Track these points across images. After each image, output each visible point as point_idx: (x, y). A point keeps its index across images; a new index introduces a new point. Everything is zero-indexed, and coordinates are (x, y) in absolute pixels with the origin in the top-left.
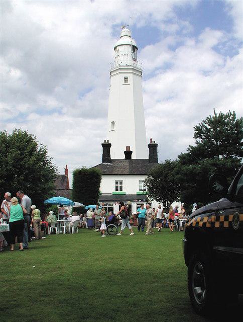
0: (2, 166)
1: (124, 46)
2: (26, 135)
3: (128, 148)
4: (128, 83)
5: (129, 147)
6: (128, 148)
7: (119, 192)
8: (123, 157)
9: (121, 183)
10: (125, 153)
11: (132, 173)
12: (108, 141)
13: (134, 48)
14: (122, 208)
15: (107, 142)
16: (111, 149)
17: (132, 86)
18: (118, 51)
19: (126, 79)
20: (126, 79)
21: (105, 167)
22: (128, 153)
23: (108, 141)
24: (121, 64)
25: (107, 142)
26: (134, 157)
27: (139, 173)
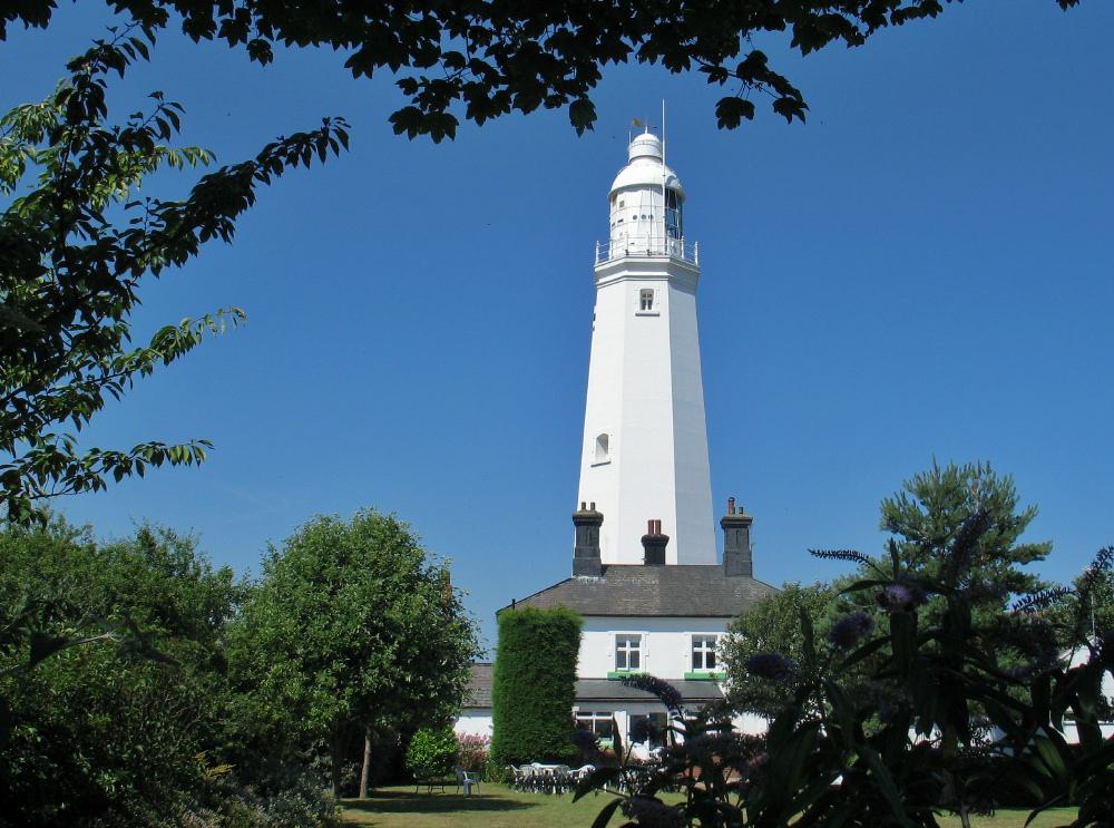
0: (926, 781)
1: (683, 614)
2: (393, 528)
3: (655, 525)
4: (654, 309)
5: (659, 522)
6: (655, 525)
7: (628, 671)
8: (637, 556)
9: (635, 645)
10: (646, 541)
11: (669, 616)
12: (593, 505)
13: (673, 198)
14: (1029, 688)
15: (588, 507)
16: (602, 529)
17: (665, 319)
18: (622, 204)
19: (646, 299)
20: (646, 299)
21: (585, 590)
22: (654, 544)
23: (593, 505)
24: (632, 250)
25: (588, 507)
26: (672, 556)
27: (692, 612)
